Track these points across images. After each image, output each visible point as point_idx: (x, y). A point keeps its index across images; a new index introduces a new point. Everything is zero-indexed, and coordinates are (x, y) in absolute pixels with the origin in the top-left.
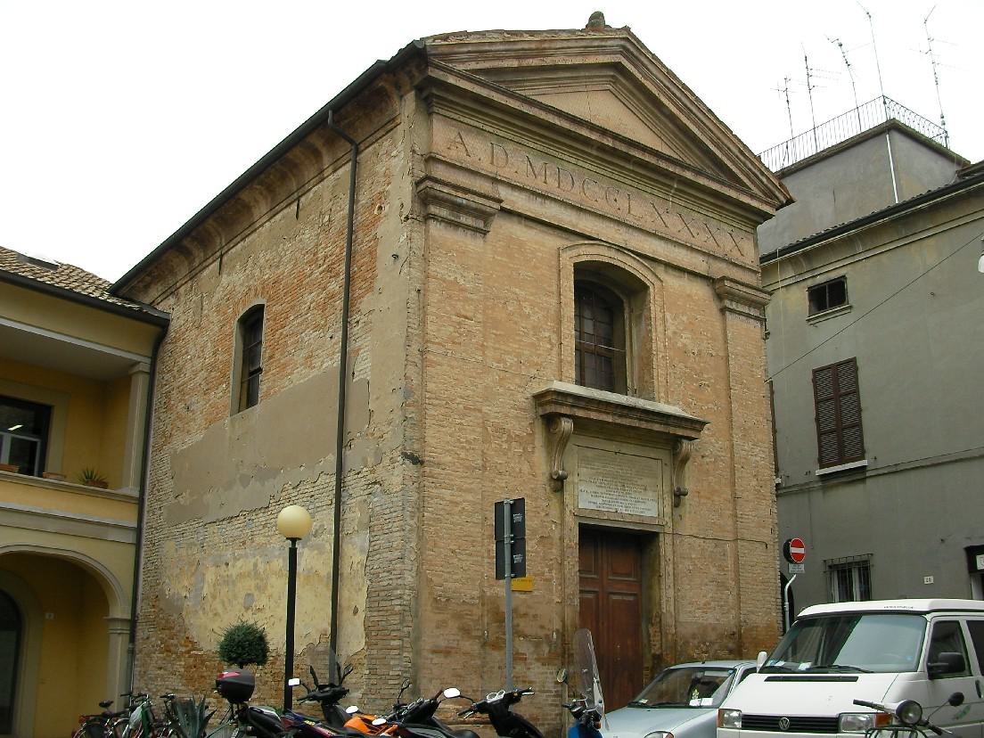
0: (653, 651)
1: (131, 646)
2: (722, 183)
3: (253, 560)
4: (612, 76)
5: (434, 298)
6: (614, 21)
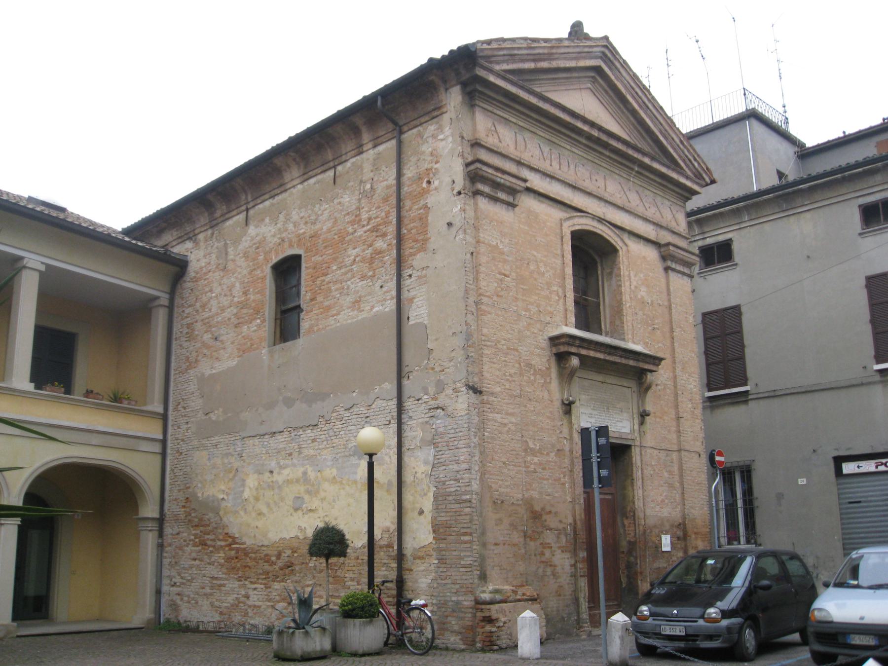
0: (628, 539)
1: (160, 541)
2: (668, 167)
3: (302, 469)
4: (593, 77)
5: (483, 259)
6: (593, 30)
